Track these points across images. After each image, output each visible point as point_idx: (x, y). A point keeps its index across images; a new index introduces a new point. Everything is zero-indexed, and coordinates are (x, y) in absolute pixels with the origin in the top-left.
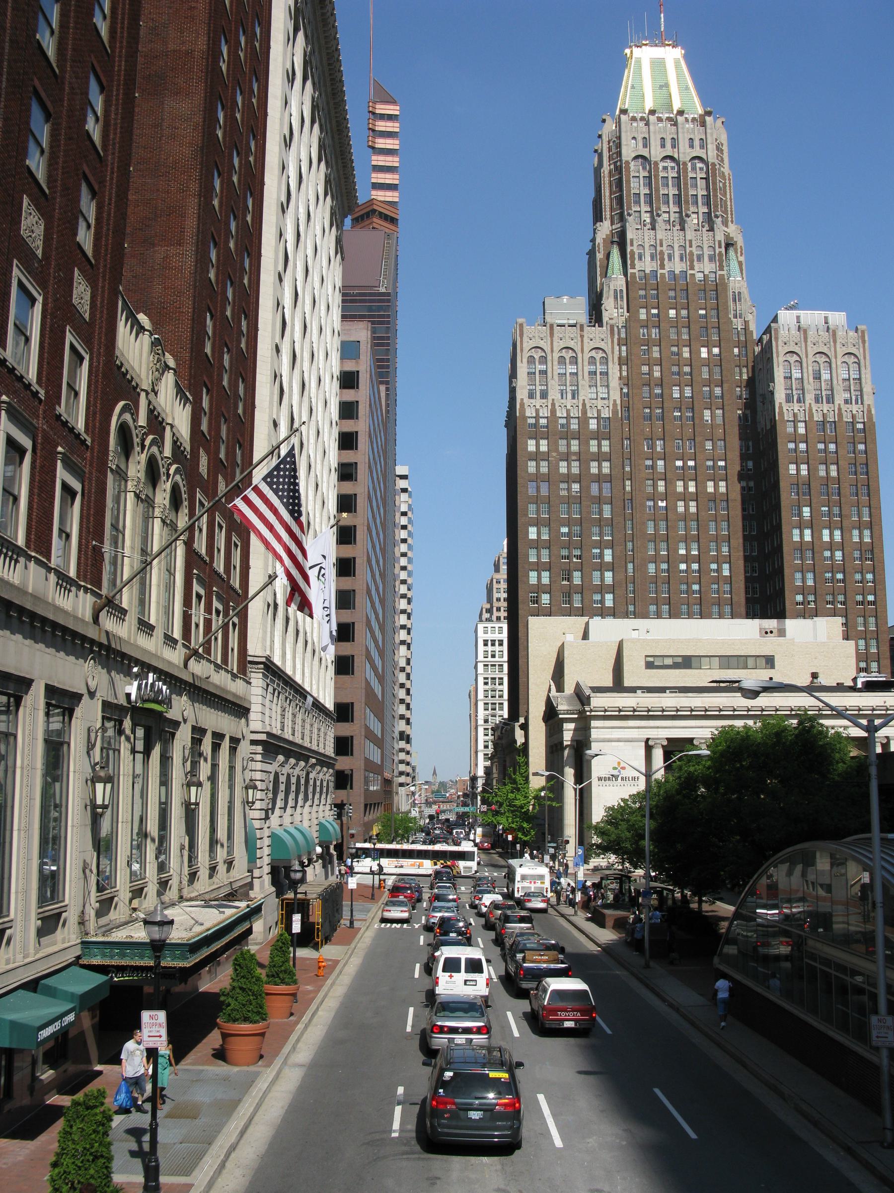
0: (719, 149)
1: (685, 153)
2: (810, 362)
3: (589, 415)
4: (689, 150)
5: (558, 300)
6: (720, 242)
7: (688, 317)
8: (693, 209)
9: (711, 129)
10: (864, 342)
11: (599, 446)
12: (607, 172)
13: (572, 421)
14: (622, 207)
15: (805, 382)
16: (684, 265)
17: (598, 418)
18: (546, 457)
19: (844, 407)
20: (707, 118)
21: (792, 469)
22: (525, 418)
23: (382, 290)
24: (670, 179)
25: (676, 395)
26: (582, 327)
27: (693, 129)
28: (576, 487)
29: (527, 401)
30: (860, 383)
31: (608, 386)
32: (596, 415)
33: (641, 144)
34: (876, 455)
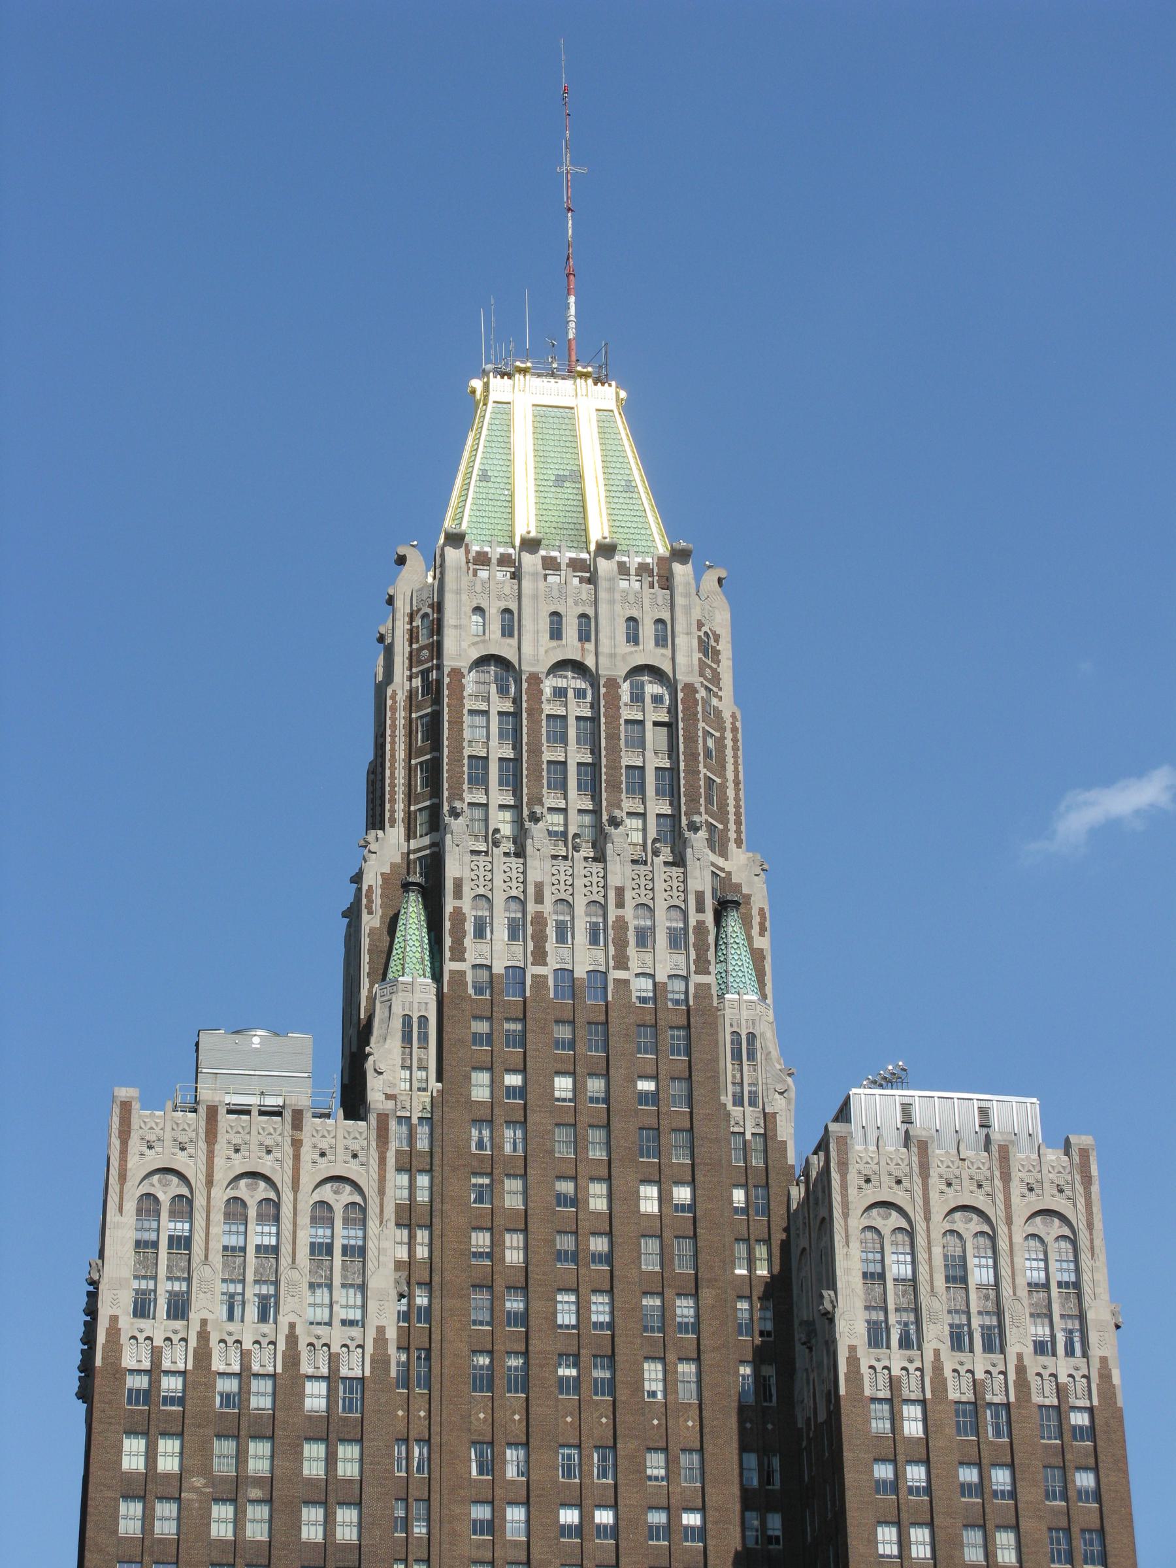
0: (707, 647)
1: (614, 655)
2: (936, 1235)
3: (306, 1368)
4: (624, 648)
5: (237, 1038)
6: (700, 896)
7: (607, 1100)
9: (687, 595)
10: (1087, 1181)
12: (401, 697)
13: (256, 1385)
15: (923, 1289)
16: (600, 955)
17: (332, 1379)
18: (171, 1489)
19: (1033, 1364)
20: (678, 568)
22: (118, 1373)
24: (572, 722)
25: (566, 1317)
26: (298, 1115)
27: (639, 597)
29: (127, 1323)
30: (1079, 1297)
31: (363, 1288)
32: (324, 1371)
33: (495, 626)
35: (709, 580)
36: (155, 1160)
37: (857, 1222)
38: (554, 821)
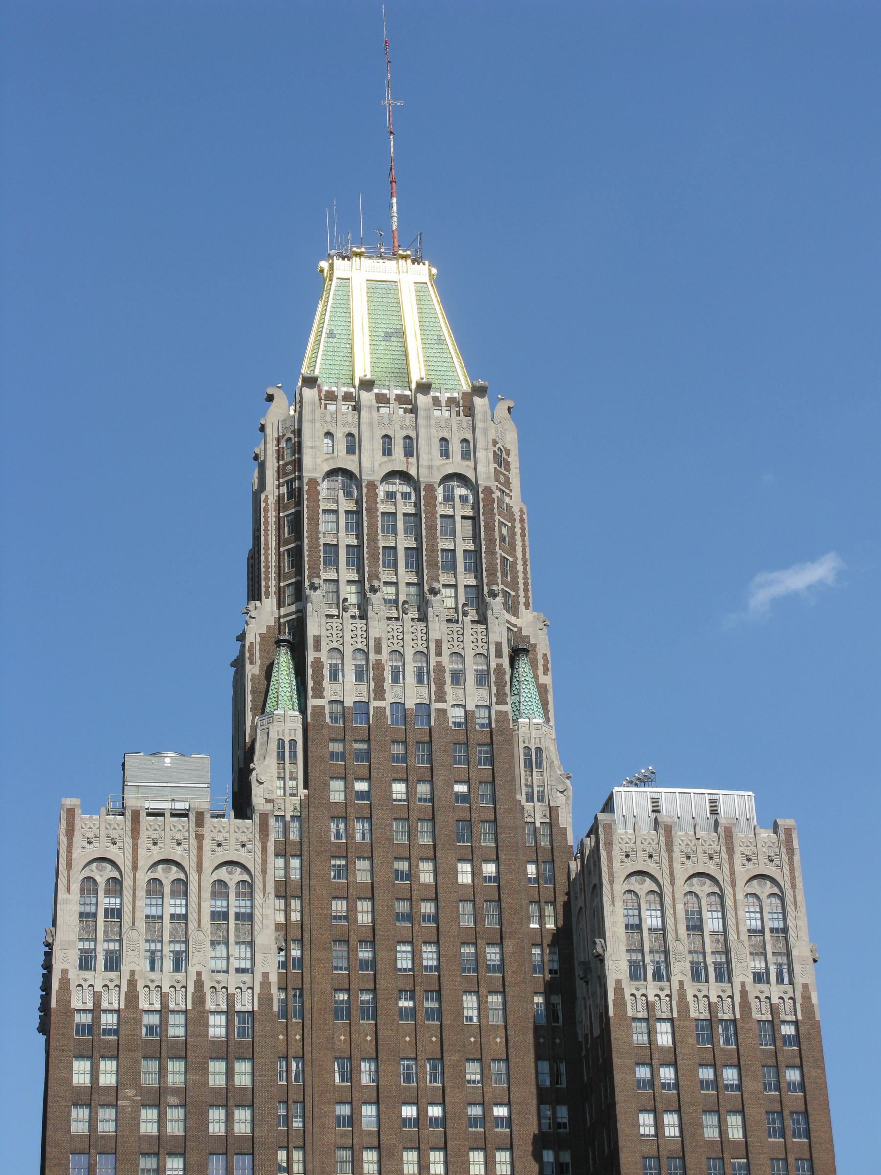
0: (500, 459)
1: (431, 466)
2: (679, 895)
3: (210, 1005)
4: (438, 461)
5: (153, 759)
6: (498, 646)
8: (444, 578)
9: (485, 421)
10: (791, 852)
12: (272, 501)
13: (172, 1019)
14: (299, 571)
15: (670, 936)
16: (425, 691)
17: (229, 1013)
18: (107, 1098)
19: (753, 990)
20: (477, 400)
21: (646, 1123)
22: (69, 1012)
24: (400, 517)
25: (404, 963)
26: (200, 816)
27: (448, 422)
29: (75, 975)
30: (786, 939)
31: (251, 944)
33: (342, 447)
34: (826, 1094)
35: (501, 409)
36: (93, 851)
37: (620, 887)
38: (389, 592)
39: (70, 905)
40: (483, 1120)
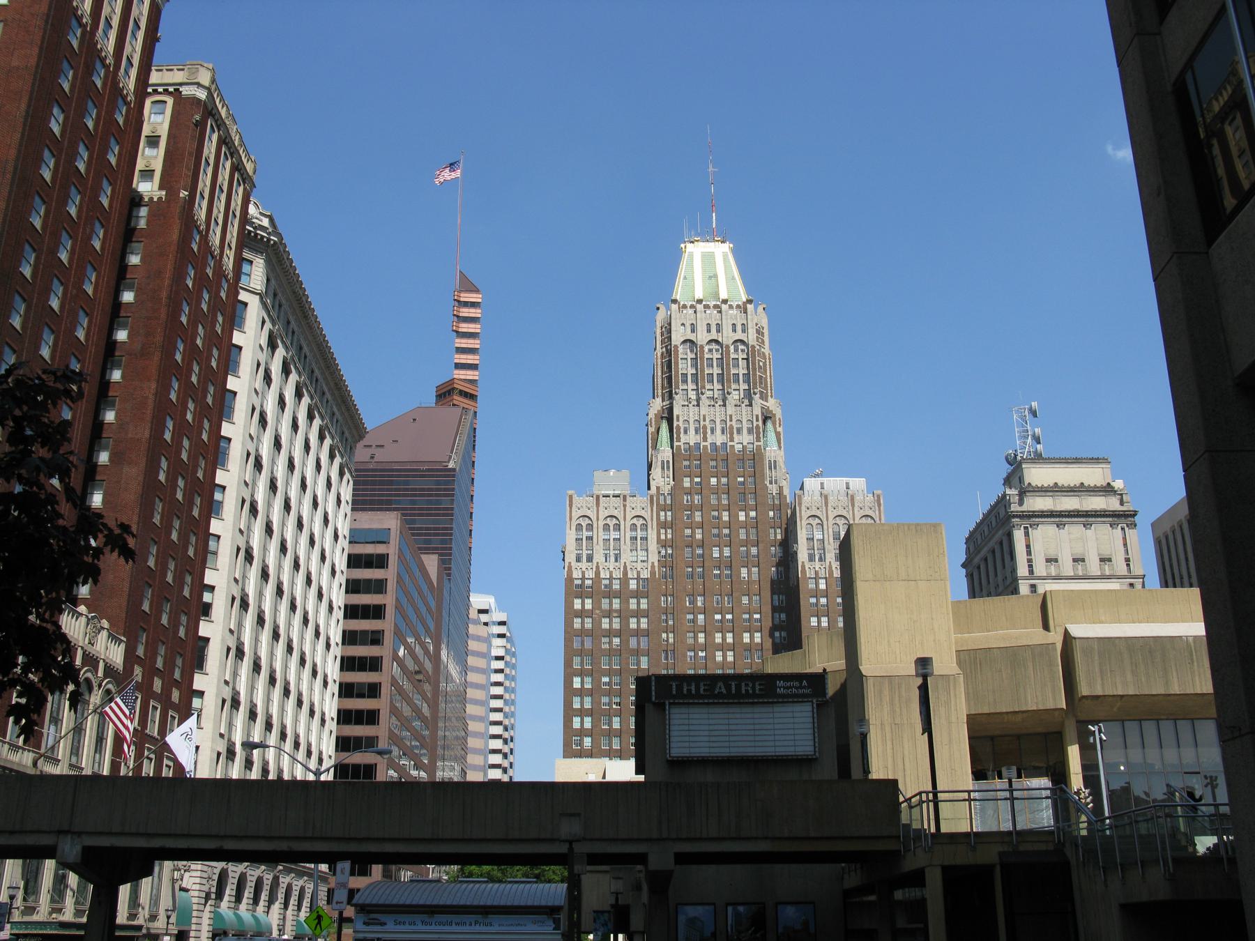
1: (728, 337)
3: (630, 575)
4: (731, 334)
10: (879, 505)
11: (638, 603)
17: (638, 579)
18: (590, 614)
23: (451, 465)
25: (716, 555)
26: (625, 497)
28: (616, 641)
29: (574, 564)
35: (760, 309)
36: (581, 513)
37: (804, 522)
38: (709, 394)
39: (571, 536)
40: (749, 620)
